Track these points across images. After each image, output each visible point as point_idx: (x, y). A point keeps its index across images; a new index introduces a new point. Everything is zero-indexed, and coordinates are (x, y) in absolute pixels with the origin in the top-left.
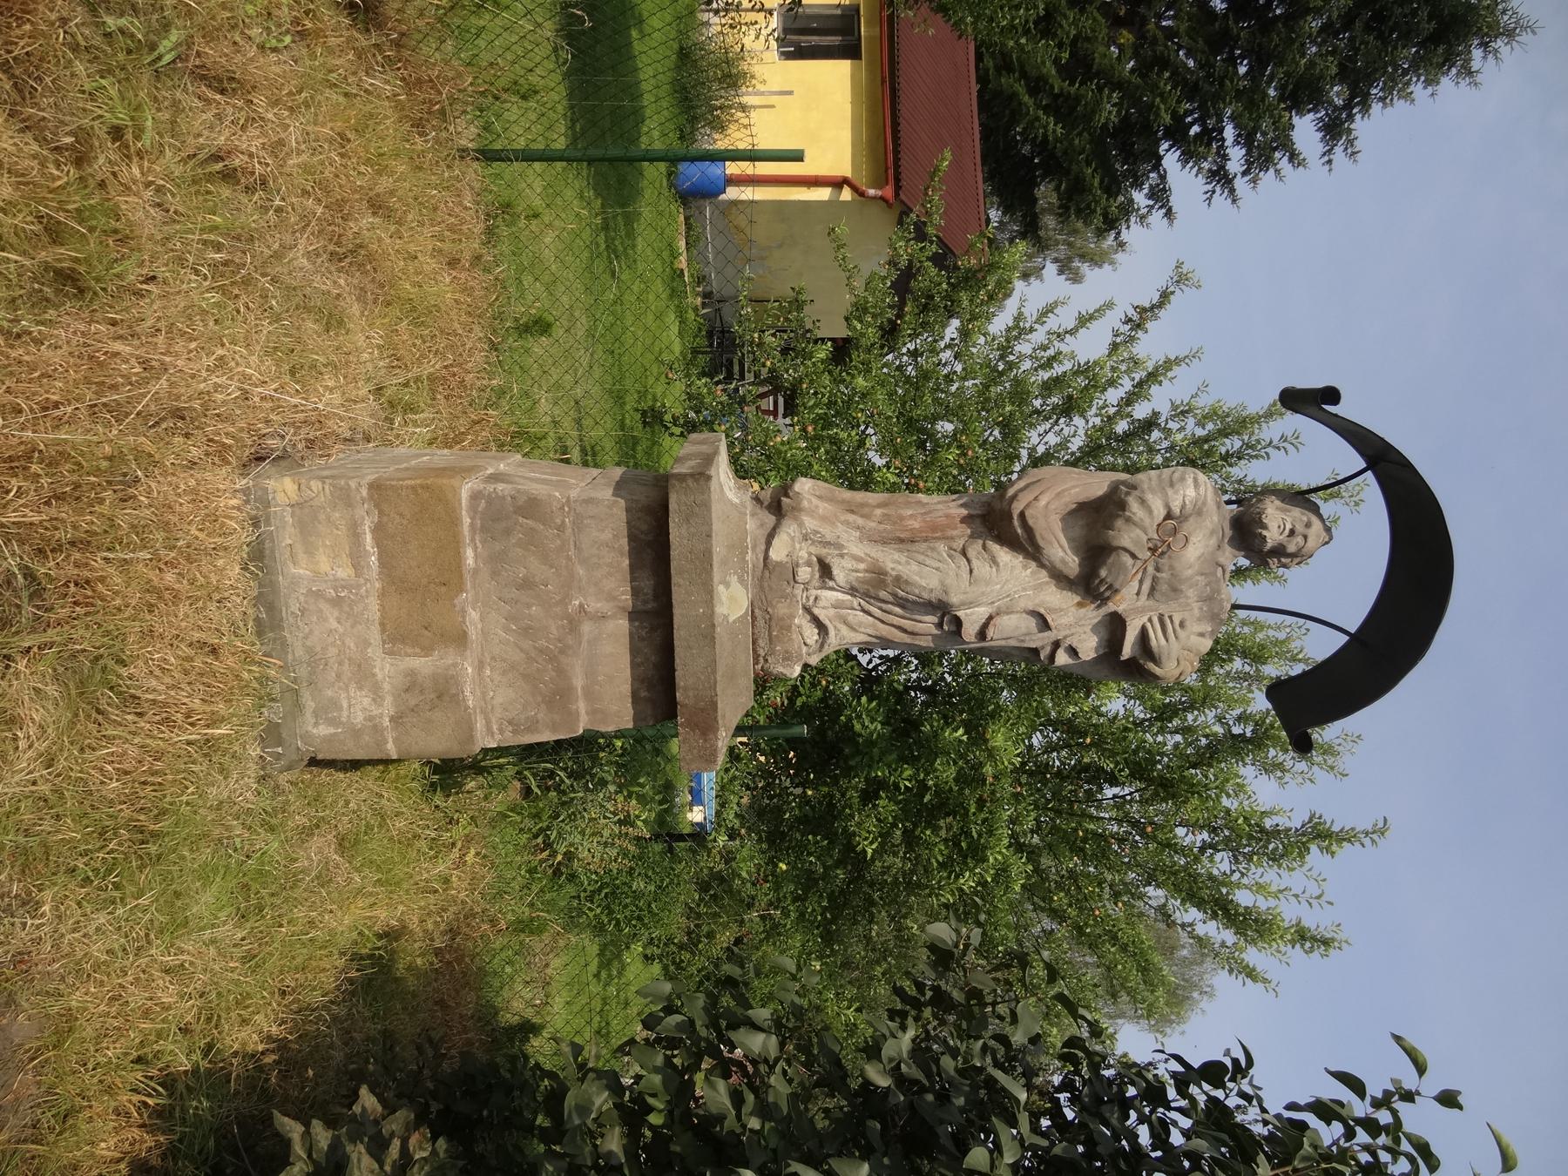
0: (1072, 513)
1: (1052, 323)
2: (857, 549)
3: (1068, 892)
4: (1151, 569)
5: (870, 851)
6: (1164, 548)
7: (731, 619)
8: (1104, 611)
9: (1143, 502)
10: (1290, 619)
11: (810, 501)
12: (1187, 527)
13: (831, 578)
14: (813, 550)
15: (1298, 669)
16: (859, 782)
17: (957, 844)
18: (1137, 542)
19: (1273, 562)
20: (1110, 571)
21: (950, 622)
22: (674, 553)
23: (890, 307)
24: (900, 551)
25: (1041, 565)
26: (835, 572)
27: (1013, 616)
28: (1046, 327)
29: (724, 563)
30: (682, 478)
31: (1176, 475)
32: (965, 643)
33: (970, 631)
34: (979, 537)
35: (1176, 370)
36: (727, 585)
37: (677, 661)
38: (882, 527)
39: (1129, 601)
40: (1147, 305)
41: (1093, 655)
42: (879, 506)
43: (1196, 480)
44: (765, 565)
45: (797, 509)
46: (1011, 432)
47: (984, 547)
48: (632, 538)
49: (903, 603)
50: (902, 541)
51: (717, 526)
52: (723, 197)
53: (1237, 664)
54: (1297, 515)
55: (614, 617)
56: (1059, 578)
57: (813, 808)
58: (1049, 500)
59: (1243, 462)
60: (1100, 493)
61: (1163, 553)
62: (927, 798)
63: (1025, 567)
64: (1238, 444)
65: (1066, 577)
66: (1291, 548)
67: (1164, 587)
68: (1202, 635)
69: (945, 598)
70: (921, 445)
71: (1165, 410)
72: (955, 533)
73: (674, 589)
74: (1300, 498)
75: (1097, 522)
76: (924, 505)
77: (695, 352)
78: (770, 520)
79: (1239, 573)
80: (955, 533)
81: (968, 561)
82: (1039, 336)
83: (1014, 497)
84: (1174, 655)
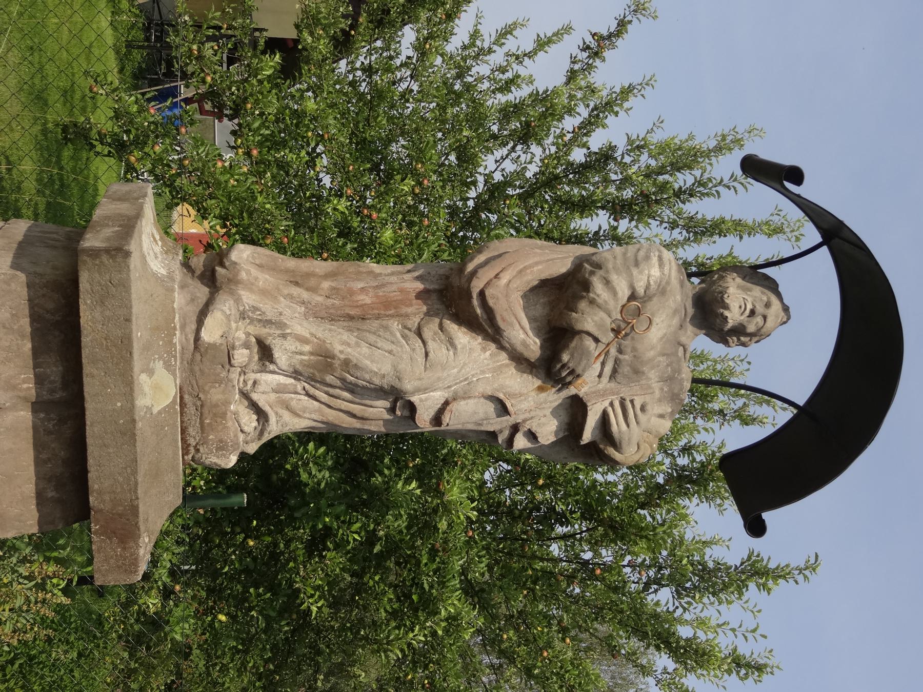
0: (533, 289)
1: (511, 44)
2: (302, 328)
3: (517, 630)
4: (613, 351)
5: (314, 609)
6: (628, 330)
7: (155, 410)
9: (607, 282)
11: (248, 273)
14: (251, 329)
16: (304, 533)
17: (408, 596)
18: (600, 326)
20: (572, 355)
21: (403, 407)
22: (86, 340)
23: (345, 16)
24: (350, 330)
25: (502, 347)
26: (277, 354)
28: (505, 49)
29: (147, 348)
30: (95, 253)
32: (418, 427)
33: (424, 420)
34: (436, 315)
35: (632, 102)
36: (151, 372)
37: (91, 461)
38: (330, 302)
39: (592, 384)
40: (605, 33)
41: (552, 439)
42: (327, 276)
43: (660, 259)
44: (196, 347)
45: (234, 281)
46: (467, 158)
47: (441, 327)
48: (35, 318)
49: (352, 388)
50: (351, 318)
51: (138, 309)
54: (757, 294)
55: (13, 408)
56: (519, 360)
57: (255, 559)
58: (514, 270)
60: (563, 270)
61: (626, 335)
62: (377, 549)
63: (484, 349)
64: (690, 181)
65: (527, 360)
66: (751, 328)
67: (625, 369)
68: (661, 416)
69: (397, 384)
70: (375, 168)
71: (621, 144)
73: (86, 380)
74: (755, 274)
75: (561, 298)
76: (376, 276)
77: (130, 45)
78: (203, 292)
80: (410, 310)
82: (498, 58)
83: (474, 273)
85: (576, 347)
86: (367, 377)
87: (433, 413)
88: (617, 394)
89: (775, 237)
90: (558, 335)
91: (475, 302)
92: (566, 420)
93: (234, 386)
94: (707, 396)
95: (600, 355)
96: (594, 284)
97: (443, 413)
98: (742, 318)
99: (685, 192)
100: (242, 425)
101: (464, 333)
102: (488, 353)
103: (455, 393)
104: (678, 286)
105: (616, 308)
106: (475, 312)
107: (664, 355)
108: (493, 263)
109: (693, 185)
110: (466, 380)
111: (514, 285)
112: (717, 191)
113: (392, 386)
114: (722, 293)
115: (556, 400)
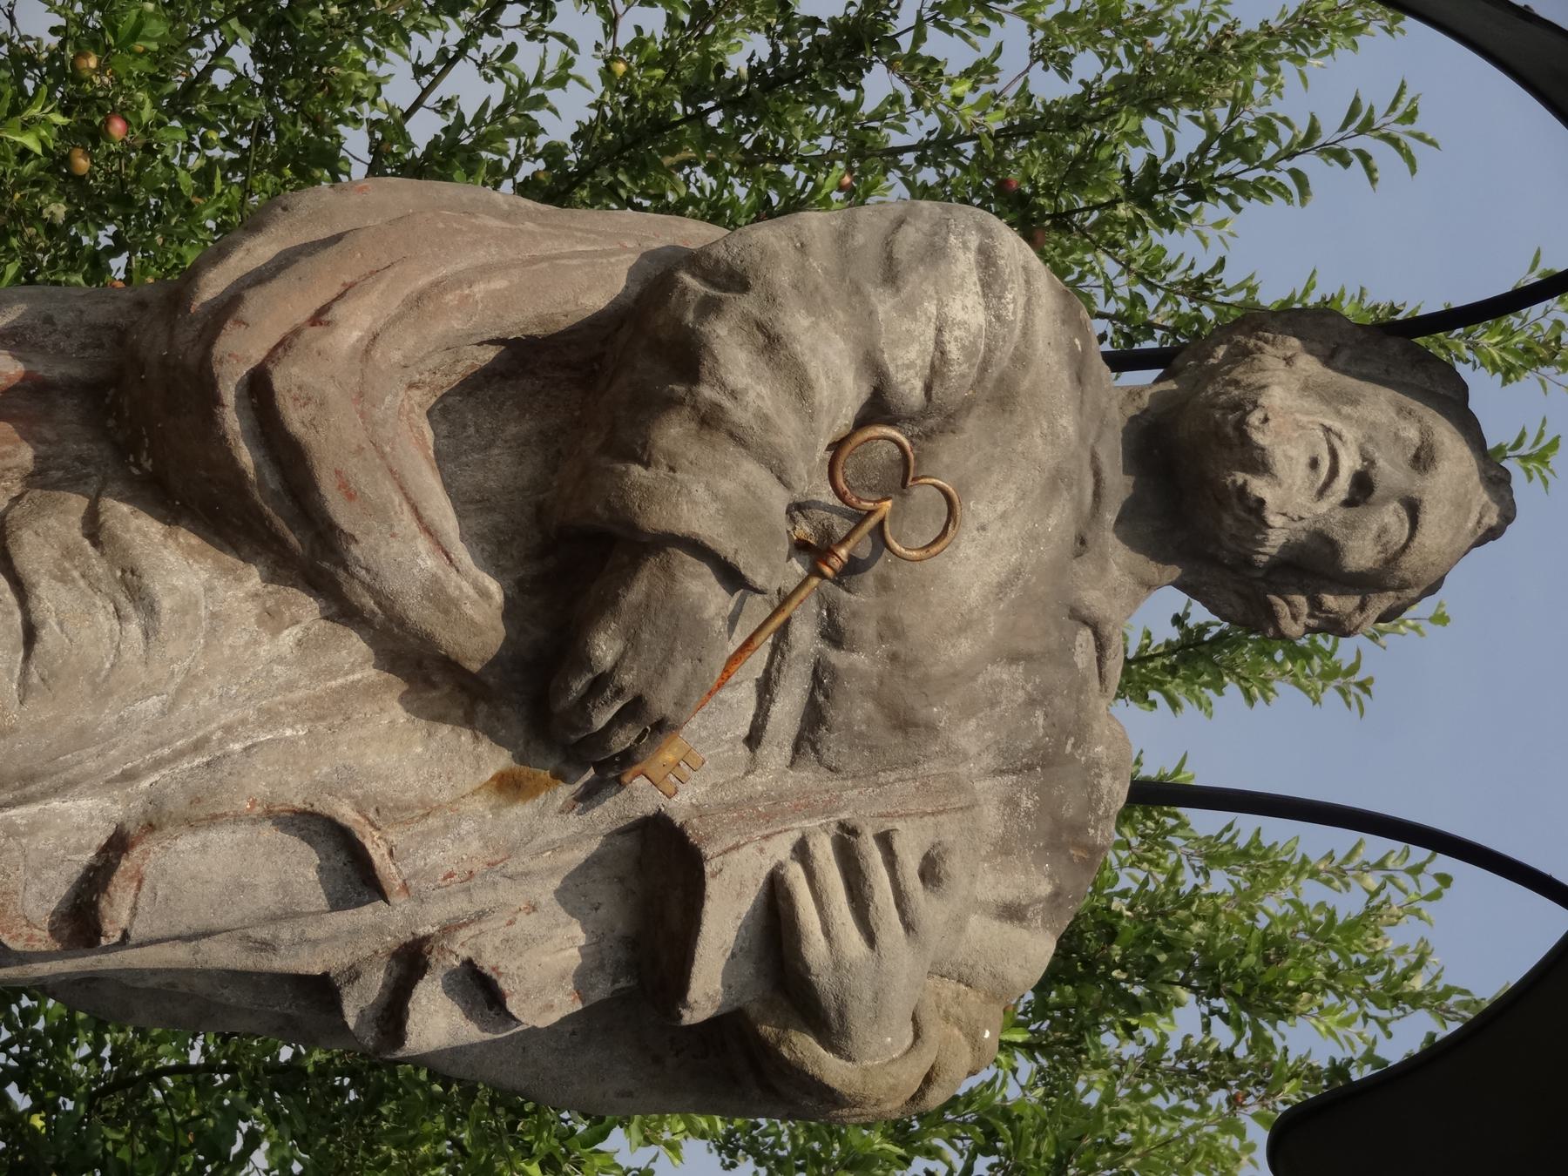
0: (477, 384)
4: (805, 635)
8: (613, 811)
9: (770, 343)
10: (1376, 846)
12: (950, 461)
15: (1407, 1036)
18: (745, 517)
19: (1293, 613)
20: (632, 640)
25: (344, 612)
27: (222, 838)
31: (910, 237)
34: (73, 482)
41: (565, 1004)
43: (987, 258)
47: (93, 528)
53: (1185, 1021)
54: (1380, 418)
56: (422, 668)
59: (1211, 211)
60: (596, 300)
61: (854, 567)
63: (272, 620)
64: (1190, 137)
65: (451, 666)
66: (1361, 554)
67: (855, 711)
68: (1012, 913)
74: (1402, 351)
75: (580, 417)
79: (1192, 658)
83: (228, 306)
84: (899, 1007)
85: (646, 606)
87: (63, 890)
88: (827, 811)
89: (1529, 380)
90: (577, 556)
91: (232, 420)
92: (620, 927)
94: (1269, 989)
95: (748, 645)
96: (717, 347)
98: (1323, 507)
99: (1170, 179)
101: (190, 552)
102: (289, 637)
103: (155, 800)
104: (1065, 377)
105: (809, 448)
106: (233, 461)
107: (1013, 659)
108: (304, 265)
109: (1204, 149)
110: (198, 747)
111: (392, 353)
112: (1296, 175)
114: (1241, 408)
115: (575, 841)
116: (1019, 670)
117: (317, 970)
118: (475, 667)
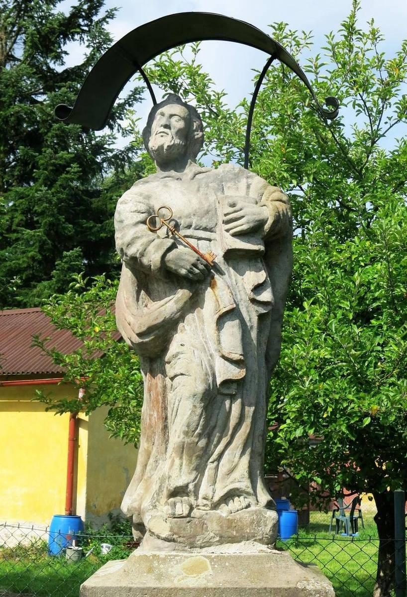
4: (189, 232)
9: (129, 245)
13: (187, 486)
20: (182, 267)
25: (182, 318)
26: (180, 483)
33: (237, 373)
38: (156, 443)
47: (169, 363)
52: (83, 519)
56: (194, 302)
65: (191, 298)
67: (204, 222)
69: (200, 396)
72: (160, 385)
81: (176, 376)
86: (196, 418)
93: (207, 514)
97: (232, 359)
100: (241, 507)
102: (186, 327)
104: (147, 185)
107: (198, 190)
113: (201, 400)
116: (201, 189)
117: (257, 318)
118: (191, 294)
